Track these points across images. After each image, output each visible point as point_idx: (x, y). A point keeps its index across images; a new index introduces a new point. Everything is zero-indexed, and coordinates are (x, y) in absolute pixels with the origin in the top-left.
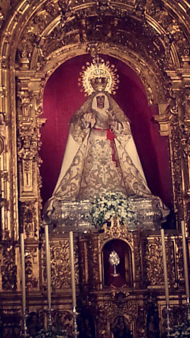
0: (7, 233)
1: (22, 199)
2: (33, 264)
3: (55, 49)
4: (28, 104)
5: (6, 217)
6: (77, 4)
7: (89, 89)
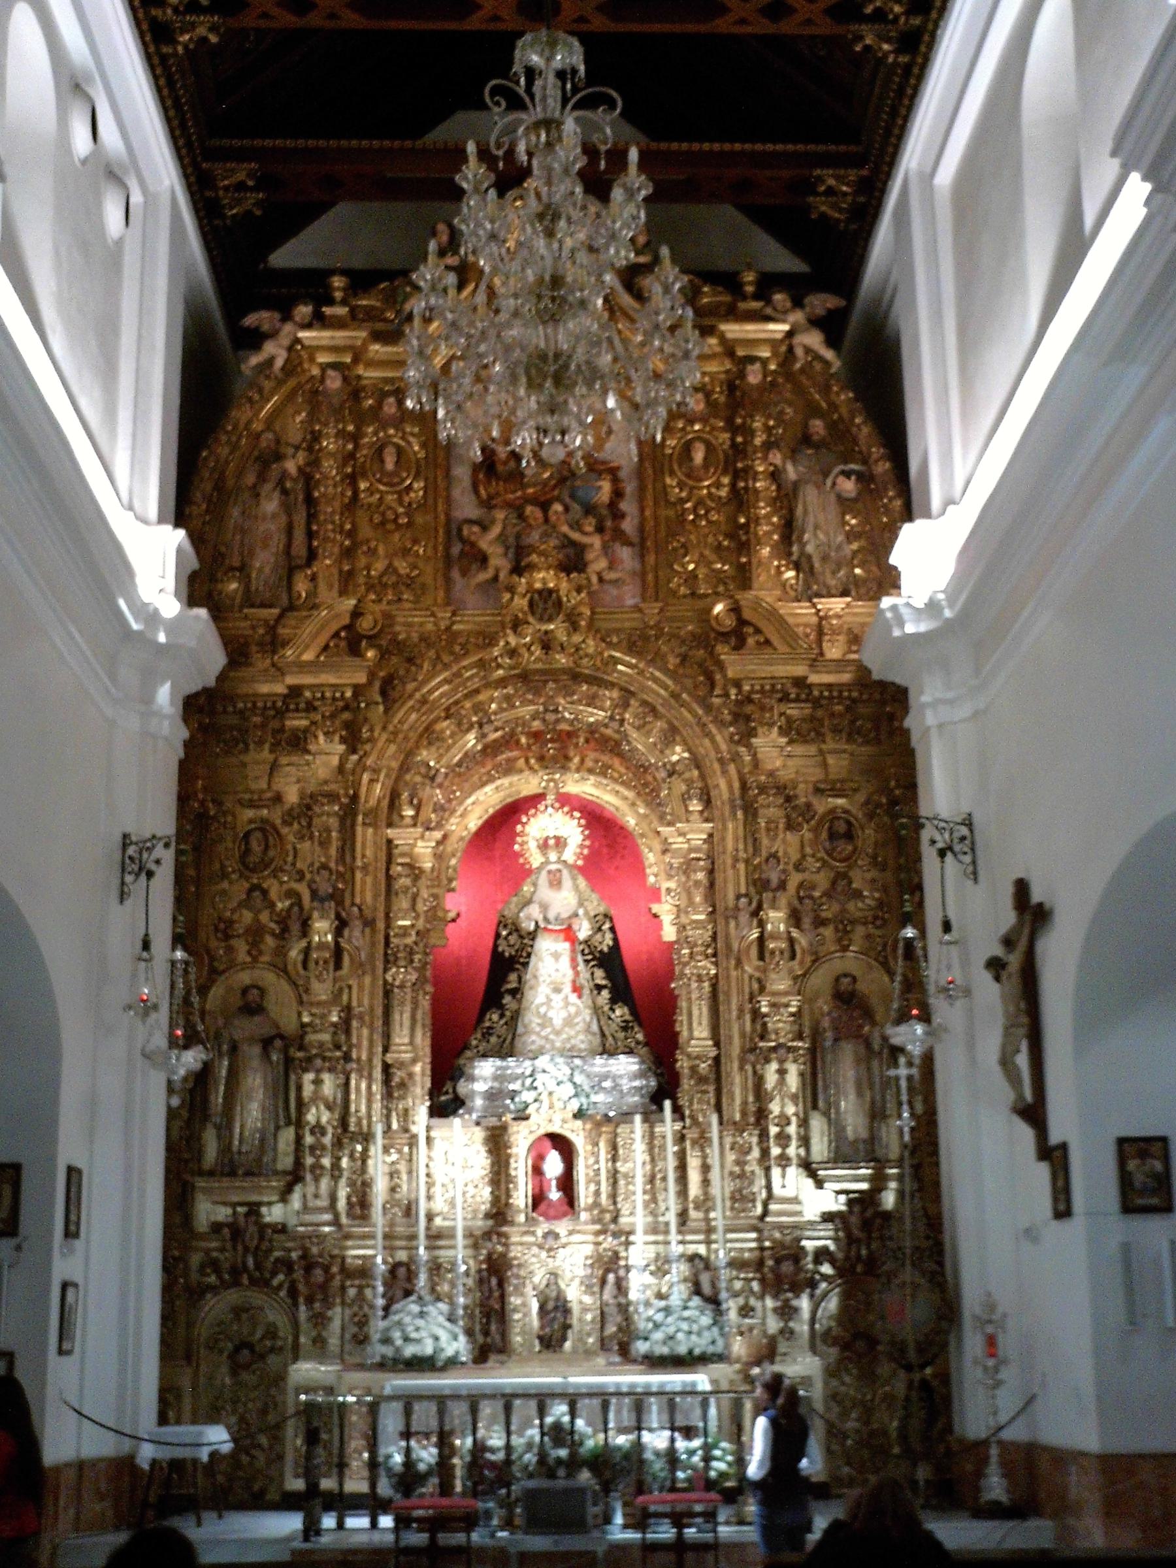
0: (360, 1120)
1: (390, 1058)
2: (734, 1273)
3: (484, 784)
4: (407, 888)
5: (358, 1089)
6: (505, 710)
7: (536, 860)
